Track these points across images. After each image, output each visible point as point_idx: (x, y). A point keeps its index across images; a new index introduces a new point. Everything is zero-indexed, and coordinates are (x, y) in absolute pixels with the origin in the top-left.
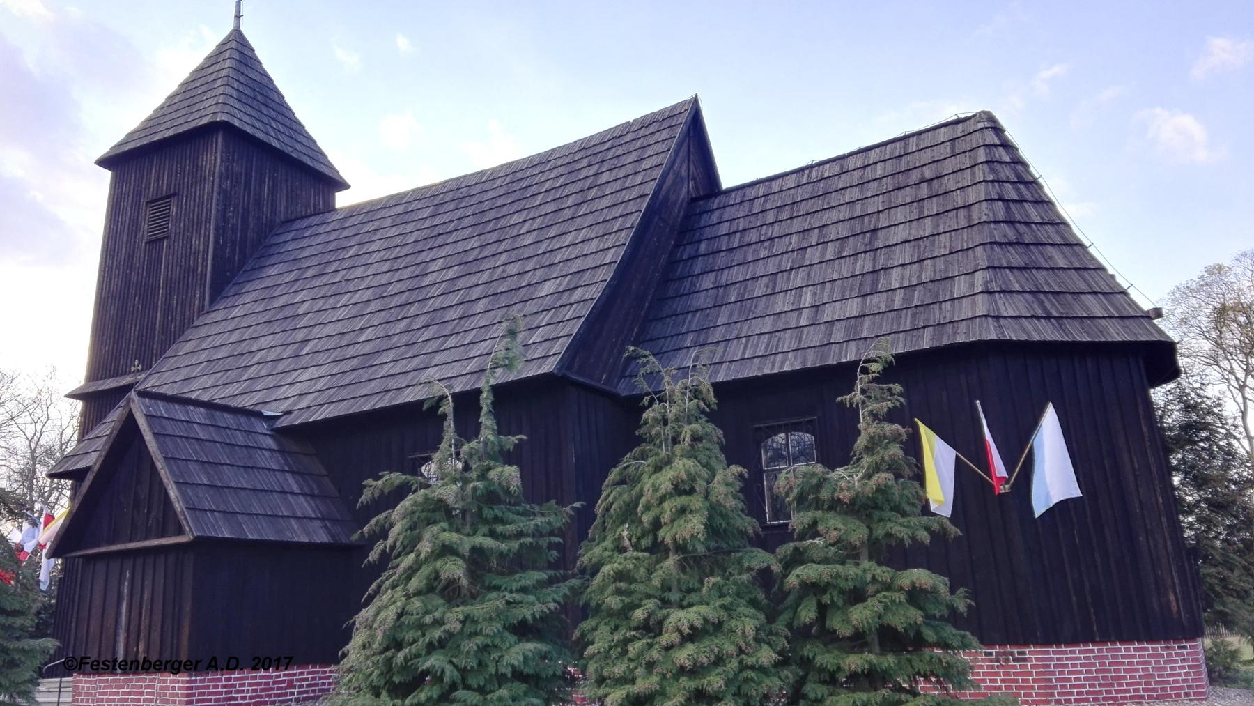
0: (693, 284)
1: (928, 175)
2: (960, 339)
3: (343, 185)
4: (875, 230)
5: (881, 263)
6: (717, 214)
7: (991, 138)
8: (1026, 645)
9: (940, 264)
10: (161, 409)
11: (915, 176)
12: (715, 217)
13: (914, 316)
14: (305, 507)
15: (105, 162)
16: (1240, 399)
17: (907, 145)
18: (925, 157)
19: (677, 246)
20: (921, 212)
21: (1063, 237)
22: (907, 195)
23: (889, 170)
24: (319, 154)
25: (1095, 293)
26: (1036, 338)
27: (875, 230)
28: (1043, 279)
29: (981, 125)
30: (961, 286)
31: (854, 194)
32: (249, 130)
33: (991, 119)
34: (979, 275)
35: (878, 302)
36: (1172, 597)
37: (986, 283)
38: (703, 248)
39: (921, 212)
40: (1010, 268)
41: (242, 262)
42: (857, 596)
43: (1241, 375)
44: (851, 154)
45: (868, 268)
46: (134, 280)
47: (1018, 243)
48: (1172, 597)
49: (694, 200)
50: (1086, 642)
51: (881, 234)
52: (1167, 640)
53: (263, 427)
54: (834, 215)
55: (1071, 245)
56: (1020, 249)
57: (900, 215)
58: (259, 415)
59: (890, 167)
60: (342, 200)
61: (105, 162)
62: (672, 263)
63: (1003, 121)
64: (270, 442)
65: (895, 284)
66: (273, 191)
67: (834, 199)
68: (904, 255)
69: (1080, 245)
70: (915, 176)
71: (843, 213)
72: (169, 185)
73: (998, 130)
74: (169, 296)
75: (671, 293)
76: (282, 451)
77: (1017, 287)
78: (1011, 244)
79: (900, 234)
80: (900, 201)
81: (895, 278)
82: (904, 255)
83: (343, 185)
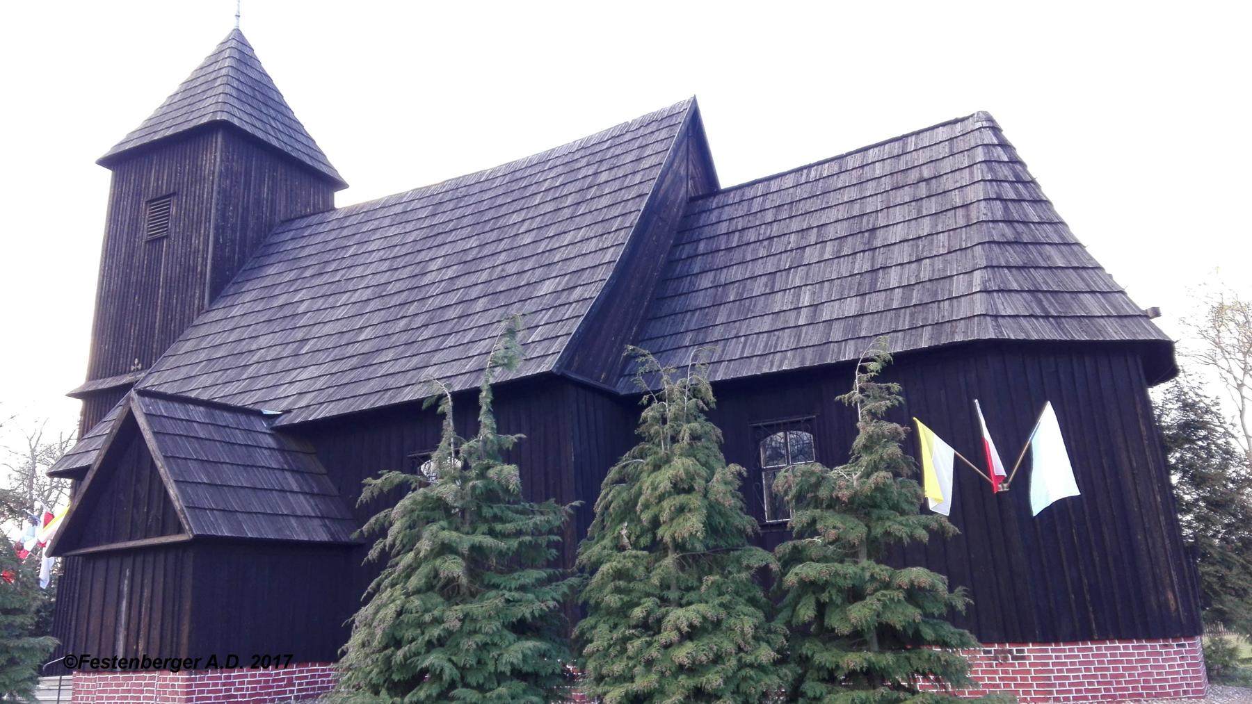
1: (926, 174)
2: (959, 338)
6: (716, 213)
7: (990, 138)
8: (1025, 643)
9: (939, 263)
10: (161, 408)
11: (913, 176)
12: (714, 217)
13: (912, 315)
14: (304, 505)
15: (106, 162)
17: (905, 144)
19: (676, 246)
20: (919, 211)
22: (905, 195)
23: (888, 170)
25: (1093, 292)
26: (1035, 337)
27: (874, 230)
29: (979, 125)
30: (959, 286)
31: (853, 193)
32: (248, 129)
34: (977, 274)
35: (876, 302)
36: (1170, 596)
37: (984, 283)
38: (702, 247)
39: (919, 211)
40: (1009, 267)
41: (242, 261)
42: (855, 594)
45: (867, 267)
46: (133, 279)
47: (1016, 242)
48: (1170, 596)
50: (1084, 640)
51: (880, 233)
52: (1165, 638)
53: (263, 426)
55: (1069, 244)
56: (1018, 248)
57: (898, 214)
58: (259, 414)
59: (888, 167)
60: (341, 200)
61: (106, 162)
62: (671, 262)
63: (1001, 123)
64: (269, 441)
65: (894, 284)
66: (272, 190)
67: (833, 199)
71: (842, 213)
74: (168, 296)
77: (1015, 286)
78: (1009, 243)
79: (898, 233)
80: (899, 201)
81: (893, 277)
82: (903, 254)
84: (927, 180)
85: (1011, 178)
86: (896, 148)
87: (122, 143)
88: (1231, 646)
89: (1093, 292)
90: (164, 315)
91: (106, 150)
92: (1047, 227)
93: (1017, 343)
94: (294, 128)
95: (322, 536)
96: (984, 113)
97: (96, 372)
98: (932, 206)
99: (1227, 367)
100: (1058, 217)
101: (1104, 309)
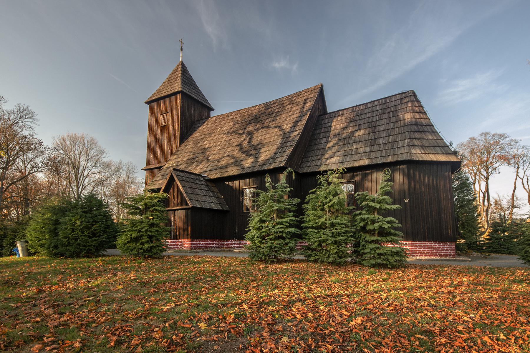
0: (320, 141)
1: (392, 110)
2: (399, 159)
3: (213, 110)
4: (375, 126)
5: (377, 136)
6: (327, 120)
7: (413, 98)
8: (407, 241)
9: (395, 137)
10: (179, 173)
11: (388, 110)
12: (326, 121)
13: (386, 152)
14: (215, 200)
15: (148, 103)
16: (474, 178)
17: (386, 100)
18: (392, 104)
19: (315, 130)
20: (390, 121)
21: (432, 130)
22: (385, 116)
23: (381, 108)
24: (206, 101)
25: (439, 147)
26: (421, 159)
27: (375, 126)
28: (425, 143)
29: (410, 94)
30: (400, 144)
31: (370, 115)
32: (188, 93)
33: (414, 93)
34: (406, 141)
35: (375, 148)
36: (449, 231)
37: (408, 143)
38: (323, 130)
39: (390, 121)
40: (415, 139)
41: (187, 132)
42: (373, 222)
43: (475, 171)
44: (369, 102)
45: (373, 137)
46: (158, 137)
47: (418, 131)
48: (449, 231)
49: (320, 116)
50: (424, 241)
51: (378, 128)
52: (446, 242)
53: (202, 179)
54: (363, 121)
55: (434, 132)
56: (419, 133)
57: (383, 122)
58: (201, 176)
59: (381, 107)
60: (213, 114)
61: (148, 103)
62: (314, 135)
63: (417, 94)
64: (204, 183)
65: (381, 143)
66: (194, 111)
67: (363, 116)
68: (384, 134)
69: (436, 132)
70: (388, 110)
71: (366, 121)
72: (166, 110)
73: (415, 95)
74: (168, 143)
75: (313, 144)
76: (208, 186)
77: (417, 144)
78: (416, 131)
79: (383, 128)
80: (384, 118)
81: (381, 141)
82: (384, 134)
83: (213, 110)
84: (393, 112)
85: (418, 111)
86: (384, 101)
87: (151, 97)
88: (469, 140)
89: (439, 147)
90: (167, 147)
91: (146, 99)
92: (428, 127)
93: (416, 161)
94: (199, 92)
95: (220, 208)
96: (413, 91)
97: (149, 162)
98: (394, 120)
99: (369, 250)
100: (431, 123)
101: (442, 151)
